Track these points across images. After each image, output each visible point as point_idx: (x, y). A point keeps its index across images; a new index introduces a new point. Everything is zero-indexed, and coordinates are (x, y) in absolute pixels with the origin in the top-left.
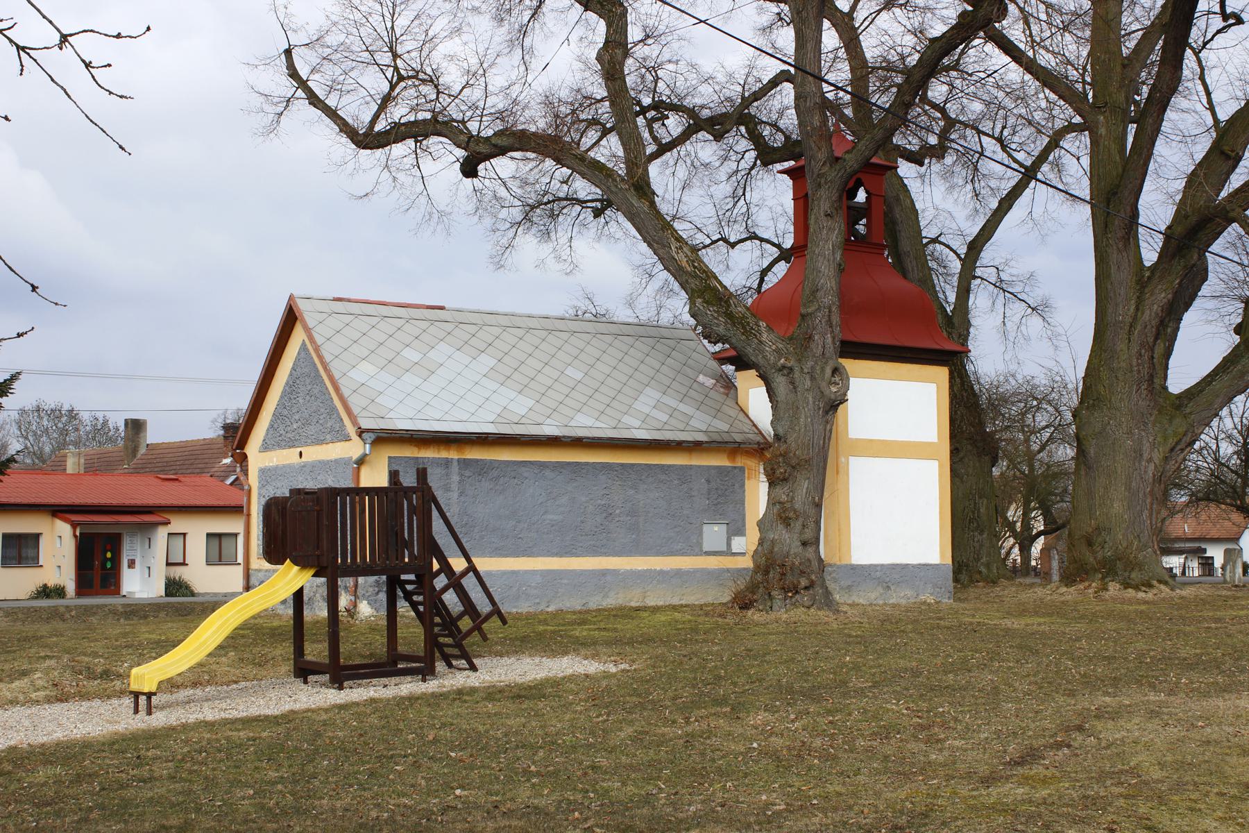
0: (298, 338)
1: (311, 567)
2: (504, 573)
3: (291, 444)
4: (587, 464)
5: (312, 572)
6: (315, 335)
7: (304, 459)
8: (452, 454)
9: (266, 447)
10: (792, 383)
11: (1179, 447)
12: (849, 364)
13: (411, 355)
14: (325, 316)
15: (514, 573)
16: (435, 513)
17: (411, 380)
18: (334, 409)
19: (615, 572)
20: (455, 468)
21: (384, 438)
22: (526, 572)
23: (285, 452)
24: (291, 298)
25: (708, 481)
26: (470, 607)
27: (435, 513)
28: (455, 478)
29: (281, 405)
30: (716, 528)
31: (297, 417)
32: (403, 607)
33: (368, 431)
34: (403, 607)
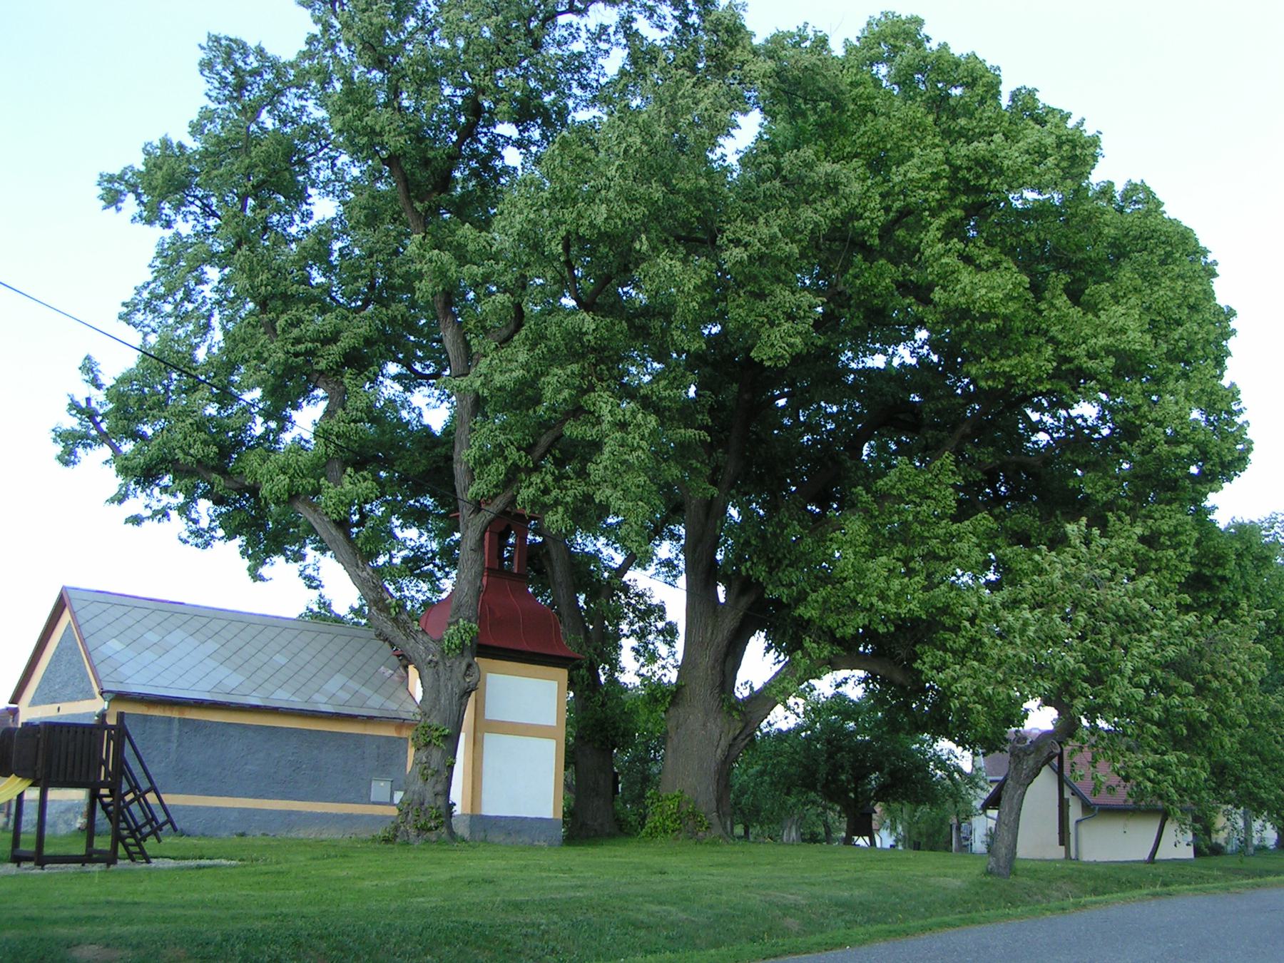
0: (66, 618)
1: (30, 778)
2: (209, 809)
3: (53, 701)
4: (282, 728)
5: (30, 782)
6: (79, 618)
7: (61, 713)
8: (175, 714)
9: (33, 703)
10: (437, 673)
11: (741, 737)
12: (482, 663)
13: (152, 637)
14: (87, 603)
15: (217, 808)
16: (127, 741)
17: (149, 656)
18: (86, 675)
19: (298, 813)
20: (176, 725)
21: (120, 697)
22: (226, 808)
23: (48, 707)
24: (64, 588)
25: (378, 747)
26: (151, 819)
27: (127, 741)
28: (176, 732)
29: (48, 670)
30: (382, 784)
31: (58, 680)
32: (100, 814)
33: (108, 692)
34: (100, 814)
